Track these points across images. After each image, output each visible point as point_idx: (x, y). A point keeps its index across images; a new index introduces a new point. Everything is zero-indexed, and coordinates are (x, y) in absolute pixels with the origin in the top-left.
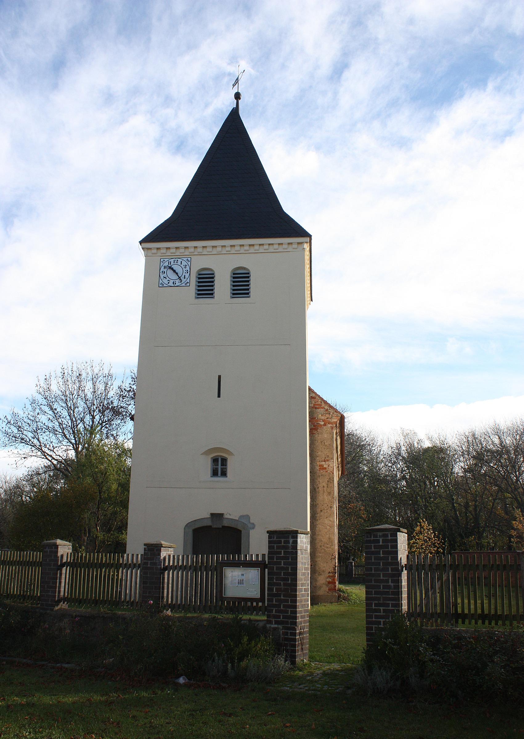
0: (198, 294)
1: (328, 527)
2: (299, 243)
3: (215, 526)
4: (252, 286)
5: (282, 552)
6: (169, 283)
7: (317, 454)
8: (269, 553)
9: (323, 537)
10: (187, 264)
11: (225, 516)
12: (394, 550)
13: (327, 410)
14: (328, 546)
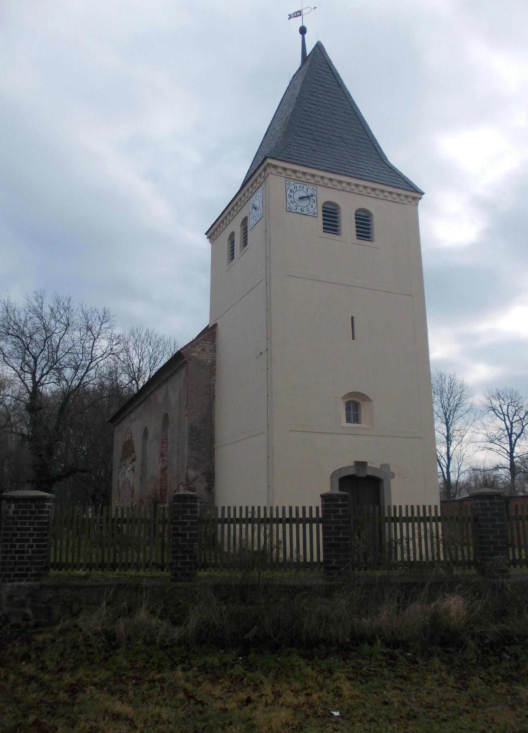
3: (360, 475)
6: (296, 209)
11: (369, 465)
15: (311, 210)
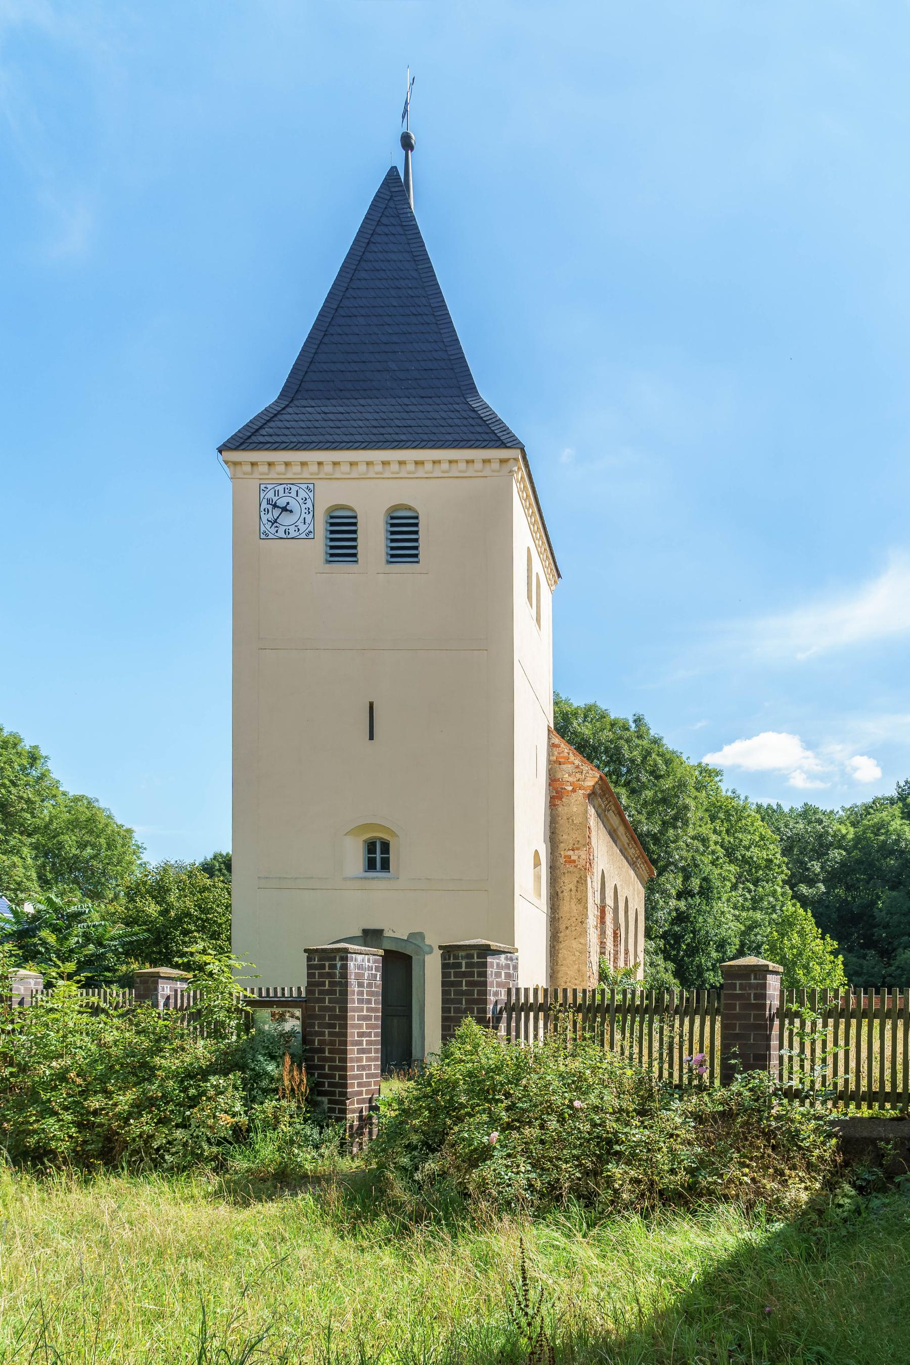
0: (393, 556)
1: (577, 954)
2: (503, 461)
4: (422, 543)
5: (327, 983)
6: (277, 532)
7: (561, 838)
8: (310, 984)
9: (569, 967)
10: (307, 497)
11: (386, 934)
12: (482, 979)
13: (577, 767)
14: (576, 981)
15: (303, 528)
